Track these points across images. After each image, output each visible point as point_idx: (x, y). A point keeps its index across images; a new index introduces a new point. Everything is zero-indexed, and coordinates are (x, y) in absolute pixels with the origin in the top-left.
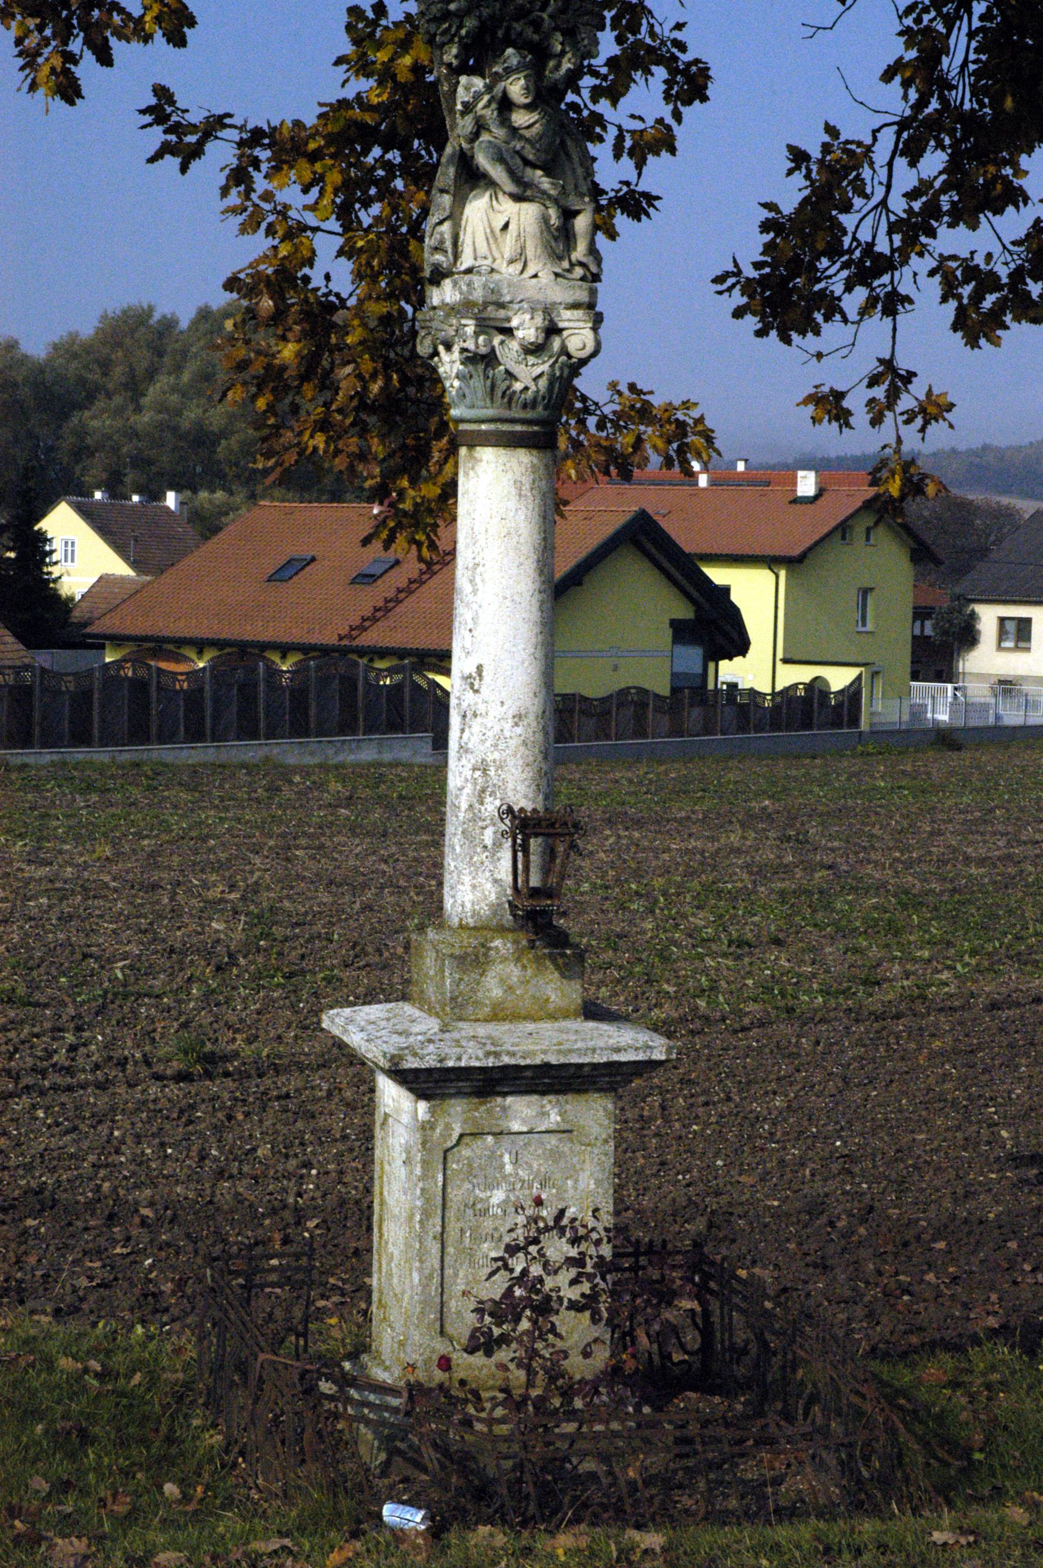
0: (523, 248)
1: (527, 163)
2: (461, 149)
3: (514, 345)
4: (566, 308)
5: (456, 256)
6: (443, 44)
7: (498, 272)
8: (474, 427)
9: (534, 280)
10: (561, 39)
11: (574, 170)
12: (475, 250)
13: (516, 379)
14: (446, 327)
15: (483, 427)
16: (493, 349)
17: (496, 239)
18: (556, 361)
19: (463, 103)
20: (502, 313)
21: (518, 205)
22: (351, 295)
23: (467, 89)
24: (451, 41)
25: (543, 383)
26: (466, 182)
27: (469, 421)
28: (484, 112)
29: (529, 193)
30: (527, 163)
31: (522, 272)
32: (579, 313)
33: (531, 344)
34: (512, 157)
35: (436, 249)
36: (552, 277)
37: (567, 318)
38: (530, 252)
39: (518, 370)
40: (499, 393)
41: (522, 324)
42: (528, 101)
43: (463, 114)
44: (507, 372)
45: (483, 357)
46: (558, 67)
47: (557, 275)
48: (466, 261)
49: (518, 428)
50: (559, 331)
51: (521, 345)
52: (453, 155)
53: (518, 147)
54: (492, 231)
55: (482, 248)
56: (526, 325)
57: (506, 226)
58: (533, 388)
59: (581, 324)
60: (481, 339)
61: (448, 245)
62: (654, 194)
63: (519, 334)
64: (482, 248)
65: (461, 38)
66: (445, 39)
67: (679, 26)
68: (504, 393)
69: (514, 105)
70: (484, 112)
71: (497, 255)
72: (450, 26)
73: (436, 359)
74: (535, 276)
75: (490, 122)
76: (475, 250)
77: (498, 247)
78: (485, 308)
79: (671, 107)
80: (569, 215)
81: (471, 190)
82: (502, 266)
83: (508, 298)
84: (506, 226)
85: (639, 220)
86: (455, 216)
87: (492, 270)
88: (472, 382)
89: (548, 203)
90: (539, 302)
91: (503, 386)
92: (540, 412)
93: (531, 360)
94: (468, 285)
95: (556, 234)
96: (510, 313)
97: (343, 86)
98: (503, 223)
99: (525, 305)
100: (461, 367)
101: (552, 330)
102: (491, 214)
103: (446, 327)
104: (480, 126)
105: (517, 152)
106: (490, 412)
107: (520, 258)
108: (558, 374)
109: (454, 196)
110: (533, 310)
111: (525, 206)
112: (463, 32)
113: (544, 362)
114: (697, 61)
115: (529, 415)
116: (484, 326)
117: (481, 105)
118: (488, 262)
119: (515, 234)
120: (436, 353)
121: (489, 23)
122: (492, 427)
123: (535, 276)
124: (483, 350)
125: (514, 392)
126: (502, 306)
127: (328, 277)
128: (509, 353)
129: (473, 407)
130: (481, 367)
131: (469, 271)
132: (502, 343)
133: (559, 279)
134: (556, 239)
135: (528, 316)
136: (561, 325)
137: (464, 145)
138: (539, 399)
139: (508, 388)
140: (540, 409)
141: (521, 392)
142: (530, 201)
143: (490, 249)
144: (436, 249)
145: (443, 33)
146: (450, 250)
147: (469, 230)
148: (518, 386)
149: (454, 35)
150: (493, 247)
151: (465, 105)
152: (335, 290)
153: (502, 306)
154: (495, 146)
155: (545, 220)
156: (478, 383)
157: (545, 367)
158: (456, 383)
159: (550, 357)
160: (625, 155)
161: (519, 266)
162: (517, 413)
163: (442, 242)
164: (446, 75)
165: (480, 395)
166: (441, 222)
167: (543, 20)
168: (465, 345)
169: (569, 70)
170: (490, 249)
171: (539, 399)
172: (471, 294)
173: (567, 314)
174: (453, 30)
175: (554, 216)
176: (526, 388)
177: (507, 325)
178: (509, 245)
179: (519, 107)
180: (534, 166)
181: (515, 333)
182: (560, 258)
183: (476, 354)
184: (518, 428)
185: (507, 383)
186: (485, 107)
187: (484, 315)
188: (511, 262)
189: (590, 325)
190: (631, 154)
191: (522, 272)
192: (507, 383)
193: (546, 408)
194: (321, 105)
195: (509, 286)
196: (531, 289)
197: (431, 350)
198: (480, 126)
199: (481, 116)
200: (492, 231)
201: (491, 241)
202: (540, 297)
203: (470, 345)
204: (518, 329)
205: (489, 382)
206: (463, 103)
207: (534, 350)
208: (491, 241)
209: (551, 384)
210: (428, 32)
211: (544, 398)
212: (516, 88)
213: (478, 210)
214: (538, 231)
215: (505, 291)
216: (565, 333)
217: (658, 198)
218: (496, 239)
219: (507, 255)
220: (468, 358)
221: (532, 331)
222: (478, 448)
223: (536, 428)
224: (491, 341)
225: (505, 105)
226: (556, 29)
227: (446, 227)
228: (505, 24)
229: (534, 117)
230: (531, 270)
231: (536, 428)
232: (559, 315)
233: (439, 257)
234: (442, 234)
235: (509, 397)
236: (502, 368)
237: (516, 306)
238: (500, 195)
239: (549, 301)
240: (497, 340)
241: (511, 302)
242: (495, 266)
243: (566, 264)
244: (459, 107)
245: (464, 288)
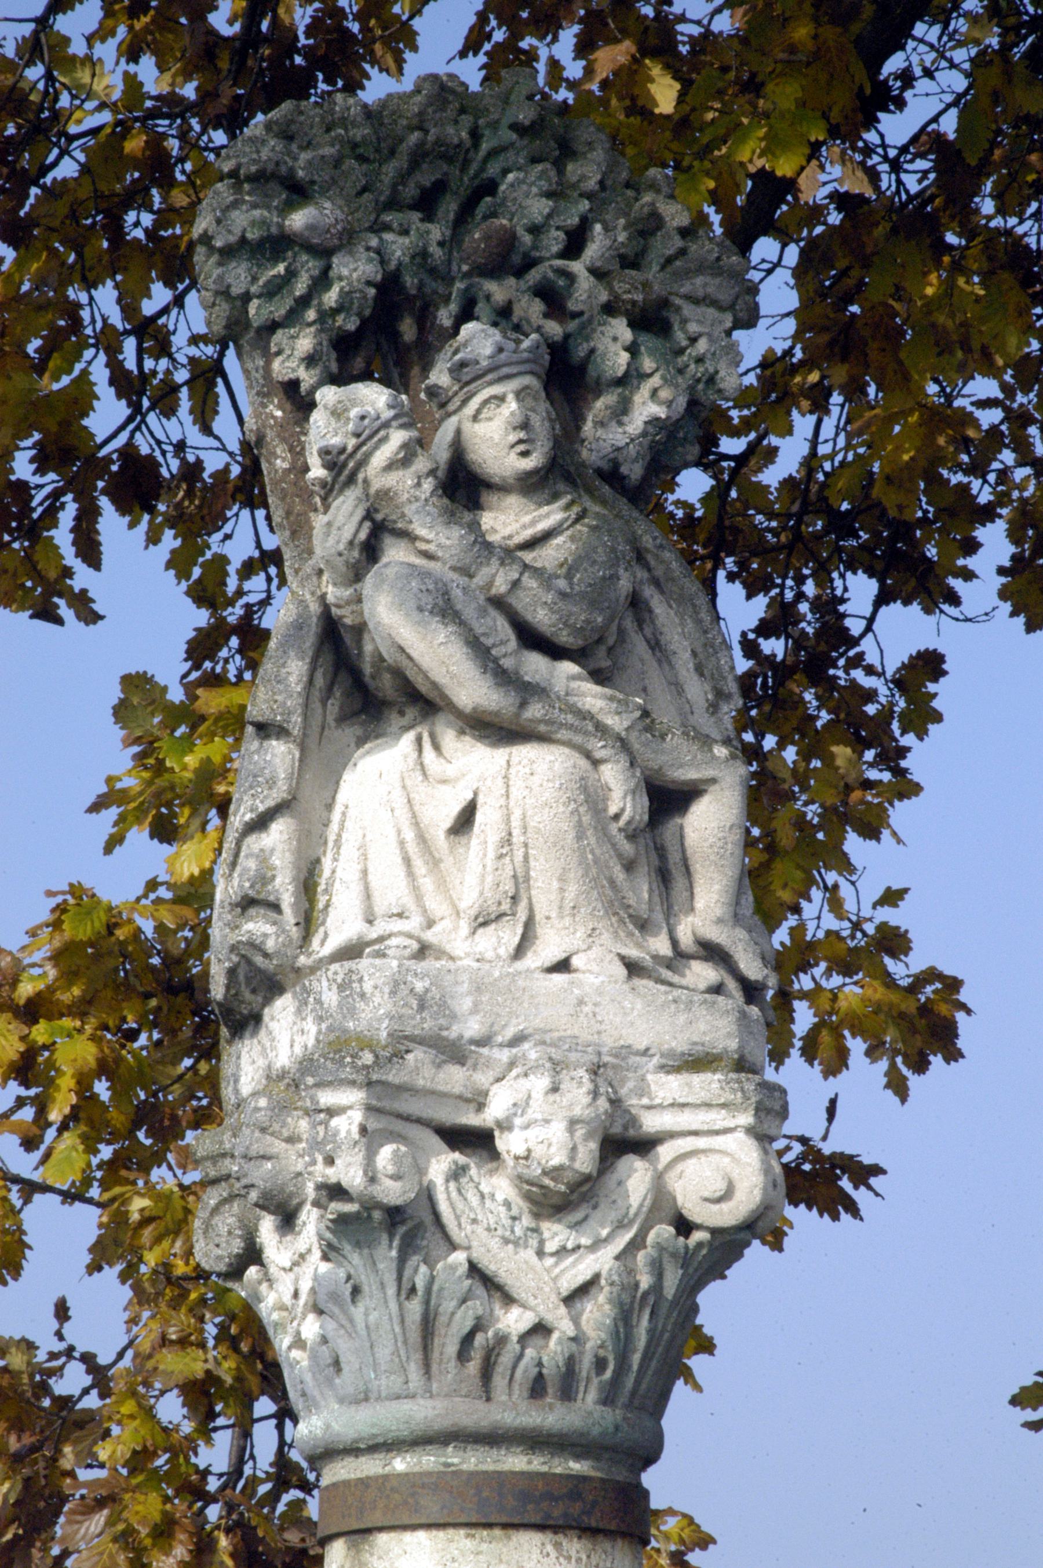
0: (521, 881)
1: (531, 638)
2: (326, 608)
3: (500, 1187)
4: (666, 1069)
5: (309, 922)
6: (273, 327)
7: (441, 953)
8: (369, 1467)
9: (558, 978)
10: (627, 335)
11: (677, 687)
12: (368, 896)
13: (509, 1300)
14: (278, 1146)
15: (400, 1464)
16: (428, 1195)
17: (434, 863)
18: (636, 1244)
19: (324, 452)
20: (454, 1078)
21: (501, 754)
22: (121, 1355)
23: (338, 413)
24: (293, 317)
25: (597, 1314)
26: (343, 719)
27: (353, 1450)
28: (391, 480)
29: (535, 711)
30: (531, 638)
31: (519, 952)
32: (708, 1084)
33: (555, 1172)
34: (483, 613)
35: (247, 904)
36: (622, 971)
37: (667, 1101)
38: (544, 894)
39: (508, 1264)
40: (448, 1345)
41: (521, 1106)
42: (529, 464)
43: (328, 490)
44: (474, 1269)
45: (395, 1215)
46: (623, 409)
47: (633, 968)
48: (342, 924)
49: (516, 1462)
50: (644, 1146)
51: (520, 1180)
52: (298, 626)
53: (501, 586)
54: (422, 838)
55: (391, 888)
56: (535, 1112)
57: (465, 821)
58: (564, 1325)
59: (718, 1119)
60: (385, 1154)
61: (284, 888)
62: (867, 1160)
63: (509, 1144)
64: (391, 888)
65: (325, 316)
66: (279, 309)
67: (892, 897)
68: (468, 1339)
69: (489, 486)
70: (391, 480)
71: (436, 905)
72: (291, 274)
73: (252, 1272)
74: (563, 966)
75: (409, 510)
76: (368, 896)
77: (442, 885)
78: (399, 1055)
79: (883, 1065)
80: (668, 800)
81: (361, 742)
82: (454, 937)
83: (472, 1028)
84: (465, 821)
85: (835, 1217)
86: (305, 804)
87: (423, 951)
88: (358, 1312)
89: (599, 747)
90: (575, 1044)
91: (463, 1321)
92: (585, 1412)
93: (556, 1233)
94: (342, 988)
95: (627, 848)
96: (482, 1078)
97: (108, 849)
98: (454, 809)
99: (531, 1052)
100: (324, 1267)
101: (622, 1142)
102: (421, 791)
103: (278, 1146)
104: (378, 533)
105: (499, 603)
106: (423, 1412)
107: (510, 909)
108: (645, 1281)
109: (303, 748)
110: (557, 1066)
111: (525, 753)
112: (331, 297)
113: (597, 1244)
114: (931, 975)
115: (552, 1416)
116: (392, 1113)
117: (381, 457)
118: (413, 924)
119: (494, 838)
120: (252, 1255)
121: (410, 281)
122: (428, 1460)
123: (563, 966)
124: (392, 1192)
125: (502, 1340)
126: (454, 1052)
127: (62, 1311)
128: (481, 1209)
129: (364, 1397)
130: (387, 1253)
131: (351, 952)
132: (457, 1174)
133: (640, 983)
134: (629, 867)
135: (540, 1083)
136: (652, 1123)
137: (332, 593)
138: (586, 1364)
139: (478, 1327)
140: (589, 1398)
141: (525, 1338)
142: (543, 739)
143: (419, 898)
144: (247, 904)
145: (274, 290)
146: (287, 900)
147: (350, 851)
148: (514, 1321)
149: (304, 302)
150: (427, 884)
151: (334, 460)
152: (81, 1348)
153: (454, 1052)
154: (424, 575)
155: (592, 798)
156: (380, 1313)
157: (602, 1261)
158: (311, 1328)
159: (621, 1225)
160: (795, 1052)
161: (509, 935)
162: (511, 1409)
163: (264, 878)
164: (281, 426)
165: (384, 1353)
166: (261, 823)
167: (571, 277)
168: (332, 1174)
169: (654, 422)
170: (419, 898)
171: (586, 1364)
172: (352, 1012)
173: (671, 1087)
174: (300, 287)
175: (621, 794)
176: (541, 1329)
177: (471, 1119)
178: (475, 872)
179: (503, 489)
180: (555, 652)
181: (502, 1143)
182: (643, 926)
183: (370, 1205)
184: (516, 1462)
185: (476, 1307)
186: (390, 466)
187: (393, 1076)
188: (483, 921)
189: (746, 1119)
190: (809, 1053)
191: (519, 952)
192: (476, 1307)
193: (607, 1399)
194: (50, 894)
195: (478, 989)
196: (548, 1004)
197: (237, 1246)
198: (378, 533)
199: (385, 495)
200: (422, 838)
201: (420, 867)
202: (581, 1029)
203: (349, 1172)
204: (505, 1125)
205: (415, 1307)
206: (324, 452)
207: (560, 1198)
208: (420, 867)
209: (625, 1317)
210: (225, 293)
211: (600, 1364)
212: (495, 430)
213: (383, 783)
214: (567, 826)
215: (466, 1004)
216: (665, 1152)
217: (877, 1170)
218: (434, 863)
219: (469, 898)
220: (342, 1222)
221: (557, 1130)
222: (383, 1539)
223: (576, 1467)
224: (421, 1171)
225: (463, 486)
226: (610, 309)
227: (278, 835)
228: (459, 285)
229: (551, 515)
230: (549, 947)
231: (576, 1467)
232: (643, 1090)
233: (256, 926)
234: (263, 858)
235: (483, 1357)
236: (459, 1257)
237: (504, 1055)
238: (449, 738)
239: (609, 1042)
240: (441, 1163)
241: (483, 1041)
242: (429, 936)
243: (661, 945)
244: (317, 471)
245: (331, 998)
